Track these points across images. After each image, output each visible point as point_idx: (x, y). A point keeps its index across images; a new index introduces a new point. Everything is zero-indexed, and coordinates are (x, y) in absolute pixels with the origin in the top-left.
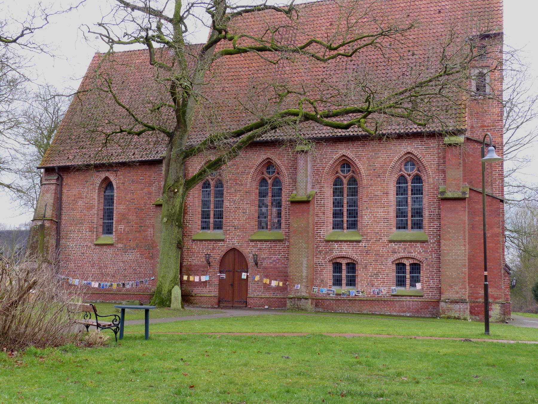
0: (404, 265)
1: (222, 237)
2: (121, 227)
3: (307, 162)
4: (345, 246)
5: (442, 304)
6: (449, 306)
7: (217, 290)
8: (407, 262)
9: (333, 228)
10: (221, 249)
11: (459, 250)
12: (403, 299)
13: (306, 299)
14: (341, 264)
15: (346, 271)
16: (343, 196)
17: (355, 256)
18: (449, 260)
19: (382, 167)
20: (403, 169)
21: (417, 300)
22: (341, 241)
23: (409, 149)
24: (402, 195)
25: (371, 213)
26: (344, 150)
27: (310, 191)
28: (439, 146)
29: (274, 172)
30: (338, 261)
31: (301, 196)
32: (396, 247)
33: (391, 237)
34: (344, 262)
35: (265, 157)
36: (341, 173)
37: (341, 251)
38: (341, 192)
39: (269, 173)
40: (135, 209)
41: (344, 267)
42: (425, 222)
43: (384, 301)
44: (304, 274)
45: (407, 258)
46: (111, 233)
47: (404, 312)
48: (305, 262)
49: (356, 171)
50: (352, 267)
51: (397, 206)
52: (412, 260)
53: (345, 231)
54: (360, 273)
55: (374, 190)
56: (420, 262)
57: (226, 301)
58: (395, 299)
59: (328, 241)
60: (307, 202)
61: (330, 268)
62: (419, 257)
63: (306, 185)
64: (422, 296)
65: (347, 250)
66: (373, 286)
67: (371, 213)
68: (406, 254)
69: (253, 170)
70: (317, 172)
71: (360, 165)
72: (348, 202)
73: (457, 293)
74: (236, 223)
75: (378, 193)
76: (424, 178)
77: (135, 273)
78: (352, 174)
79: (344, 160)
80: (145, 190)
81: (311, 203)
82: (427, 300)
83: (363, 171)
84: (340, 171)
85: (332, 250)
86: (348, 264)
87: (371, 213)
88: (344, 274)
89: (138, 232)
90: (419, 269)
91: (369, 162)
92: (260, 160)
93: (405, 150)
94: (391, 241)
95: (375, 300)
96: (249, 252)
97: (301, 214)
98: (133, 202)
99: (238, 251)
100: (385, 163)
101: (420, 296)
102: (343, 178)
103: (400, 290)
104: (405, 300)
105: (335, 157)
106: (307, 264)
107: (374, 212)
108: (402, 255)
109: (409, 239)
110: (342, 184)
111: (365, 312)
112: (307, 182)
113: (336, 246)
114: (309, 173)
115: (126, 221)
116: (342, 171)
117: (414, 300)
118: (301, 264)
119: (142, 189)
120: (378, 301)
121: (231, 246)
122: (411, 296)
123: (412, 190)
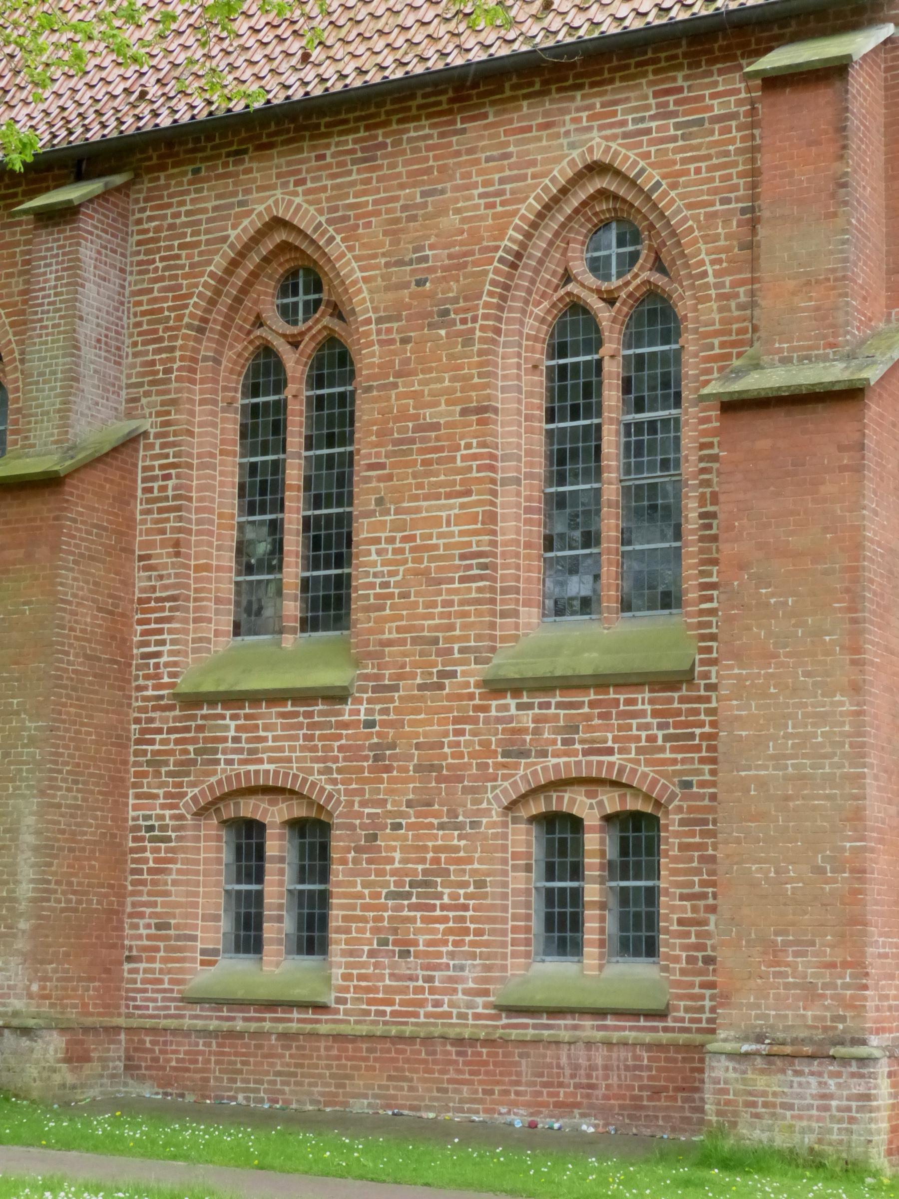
0: (576, 824)
5: (721, 1071)
6: (761, 1082)
8: (587, 807)
9: (237, 630)
11: (823, 718)
12: (562, 1029)
15: (287, 861)
16: (678, 536)
17: (323, 783)
18: (762, 784)
19: (457, 265)
20: (579, 268)
21: (631, 1035)
22: (255, 698)
23: (598, 145)
24: (575, 417)
25: (398, 526)
26: (279, 193)
30: (249, 808)
32: (527, 719)
33: (506, 663)
34: (274, 814)
43: (459, 1041)
44: (25, 890)
47: (565, 1107)
48: (30, 820)
51: (549, 482)
52: (616, 794)
53: (289, 641)
55: (415, 395)
56: (658, 804)
58: (514, 1034)
59: (193, 701)
62: (644, 773)
64: (661, 1015)
65: (277, 749)
66: (405, 954)
73: (810, 993)
75: (443, 412)
76: (684, 306)
78: (326, 321)
82: (682, 1038)
85: (208, 751)
86: (298, 826)
90: (652, 848)
91: (395, 243)
93: (575, 154)
94: (496, 687)
95: (412, 1039)
97: (21, 553)
100: (475, 237)
101: (650, 1015)
103: (554, 976)
104: (565, 1035)
105: (233, 234)
106: (38, 833)
107: (415, 524)
108: (556, 764)
109: (586, 670)
111: (359, 1106)
113: (230, 724)
117: (615, 1036)
120: (428, 1040)
122: (599, 1013)
123: (627, 386)
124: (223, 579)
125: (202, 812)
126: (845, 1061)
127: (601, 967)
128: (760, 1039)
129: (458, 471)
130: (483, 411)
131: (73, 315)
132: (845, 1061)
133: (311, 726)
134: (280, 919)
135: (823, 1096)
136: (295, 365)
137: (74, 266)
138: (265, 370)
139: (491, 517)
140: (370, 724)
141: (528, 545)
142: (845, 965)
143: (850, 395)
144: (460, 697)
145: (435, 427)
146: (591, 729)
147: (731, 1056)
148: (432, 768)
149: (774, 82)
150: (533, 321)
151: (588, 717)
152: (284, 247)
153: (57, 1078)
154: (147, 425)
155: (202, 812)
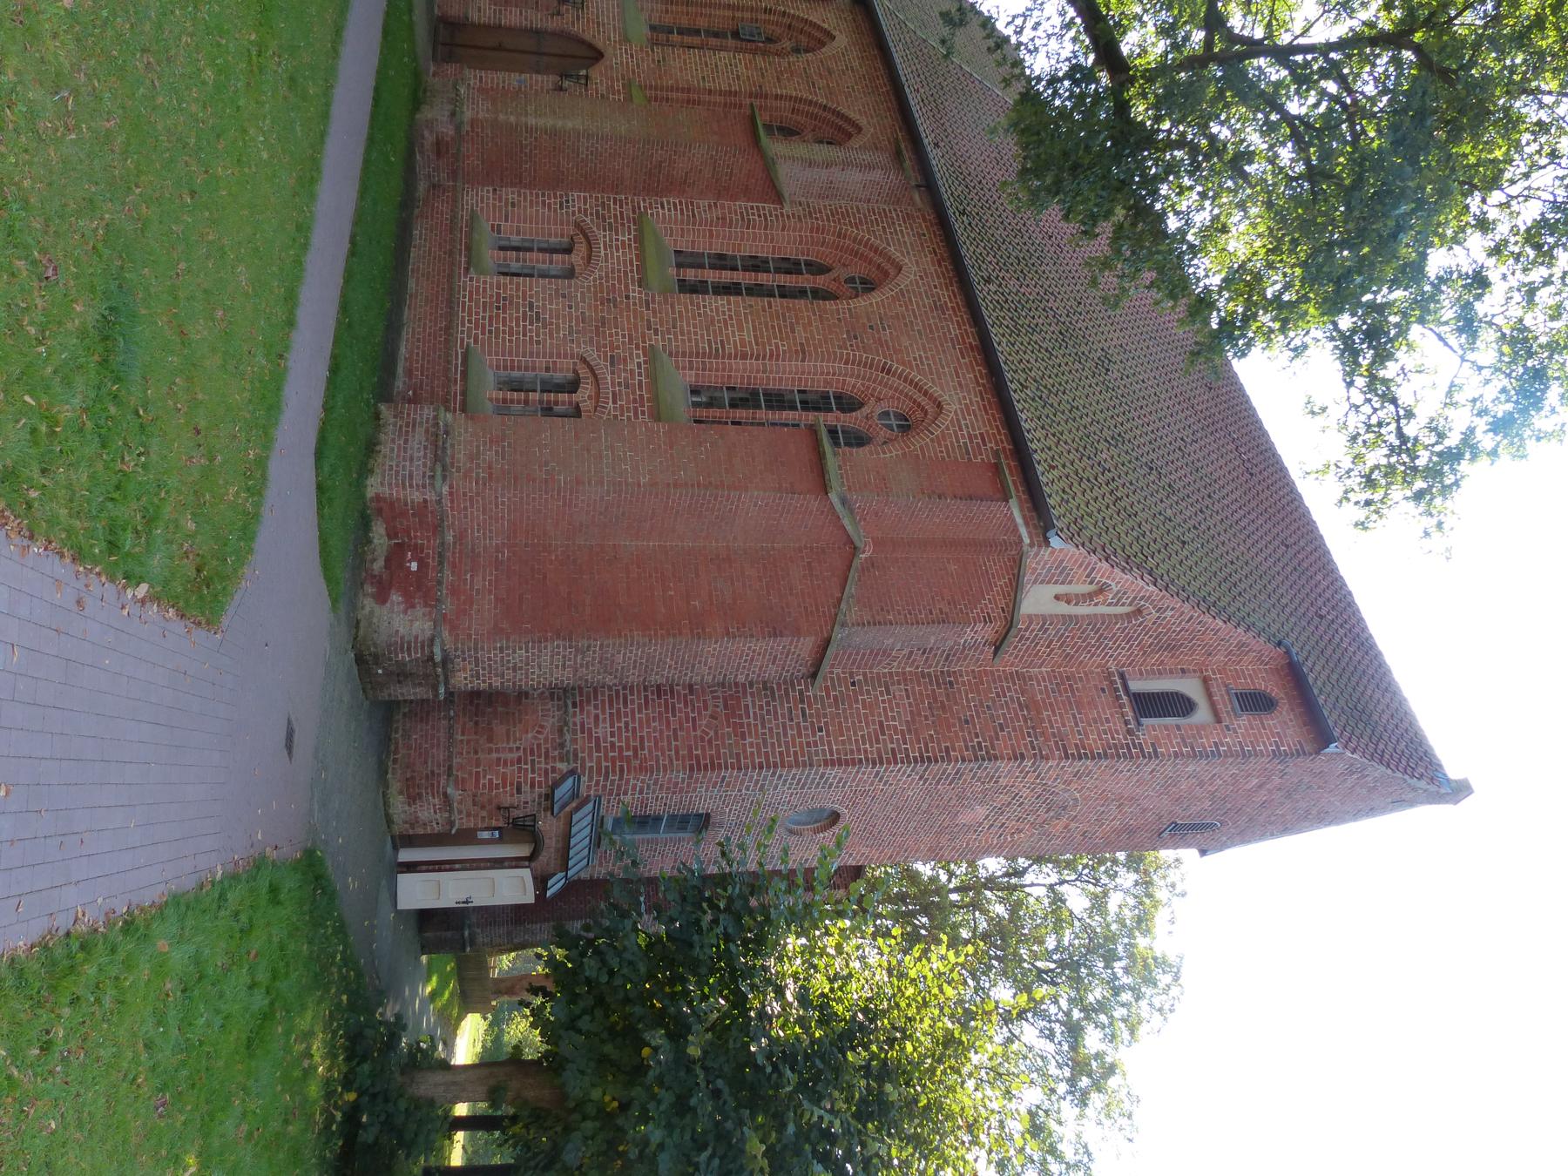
43: (448, 328)
44: (532, 121)
48: (570, 125)
53: (672, 271)
55: (810, 324)
121: (609, 52)
124: (704, 246)
125: (577, 225)
126: (433, 469)
127: (491, 400)
128: (447, 433)
129: (769, 339)
130: (803, 353)
131: (846, 164)
132: (433, 469)
133: (626, 273)
134: (518, 260)
135: (412, 459)
136: (821, 281)
137: (871, 167)
138: (817, 269)
139: (744, 357)
140: (627, 297)
141: (729, 377)
142: (490, 475)
143: (824, 488)
144: (643, 337)
145: (793, 331)
146: (627, 394)
147: (436, 418)
148: (603, 324)
149: (997, 468)
150: (852, 384)
151: (634, 393)
152: (886, 274)
153: (426, 133)
154: (787, 209)
155: (577, 225)
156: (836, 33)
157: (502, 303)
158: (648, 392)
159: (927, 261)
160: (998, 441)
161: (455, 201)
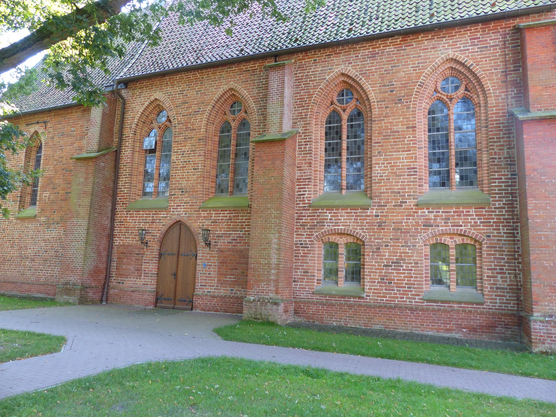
0: (446, 247)
1: (165, 205)
2: (47, 194)
3: (283, 83)
4: (343, 216)
7: (154, 282)
10: (165, 221)
13: (276, 304)
14: (337, 245)
18: (546, 237)
19: (405, 86)
22: (337, 207)
26: (343, 66)
27: (287, 127)
28: (505, 44)
29: (240, 110)
30: (333, 238)
31: (272, 134)
32: (432, 216)
35: (226, 87)
36: (338, 104)
37: (337, 224)
38: (337, 133)
39: (233, 112)
40: (63, 170)
41: (342, 250)
42: (483, 173)
43: (411, 309)
44: (274, 261)
45: (341, 234)
46: (35, 204)
48: (276, 241)
49: (363, 99)
50: (356, 251)
52: (460, 238)
54: (371, 264)
57: (165, 299)
60: (281, 141)
61: (319, 250)
62: (473, 232)
63: (281, 118)
67: (387, 160)
68: (450, 228)
69: (209, 107)
70: (301, 103)
71: (367, 87)
72: (348, 148)
74: (184, 183)
75: (400, 128)
77: (57, 256)
79: (344, 82)
80: (75, 145)
81: (289, 143)
83: (372, 96)
84: (336, 103)
85: (321, 223)
87: (387, 160)
88: (343, 263)
89: (64, 200)
91: (383, 80)
92: (220, 92)
96: (197, 225)
98: (61, 162)
99: (186, 226)
102: (342, 112)
105: (327, 77)
107: (391, 159)
110: (340, 121)
112: (282, 113)
114: (286, 101)
115: (51, 186)
116: (339, 101)
118: (269, 243)
119: (72, 144)
121: (176, 218)
156: (152, 98)
157: (386, 281)
158: (452, 208)
159: (335, 59)
160: (478, 31)
161: (305, 303)
